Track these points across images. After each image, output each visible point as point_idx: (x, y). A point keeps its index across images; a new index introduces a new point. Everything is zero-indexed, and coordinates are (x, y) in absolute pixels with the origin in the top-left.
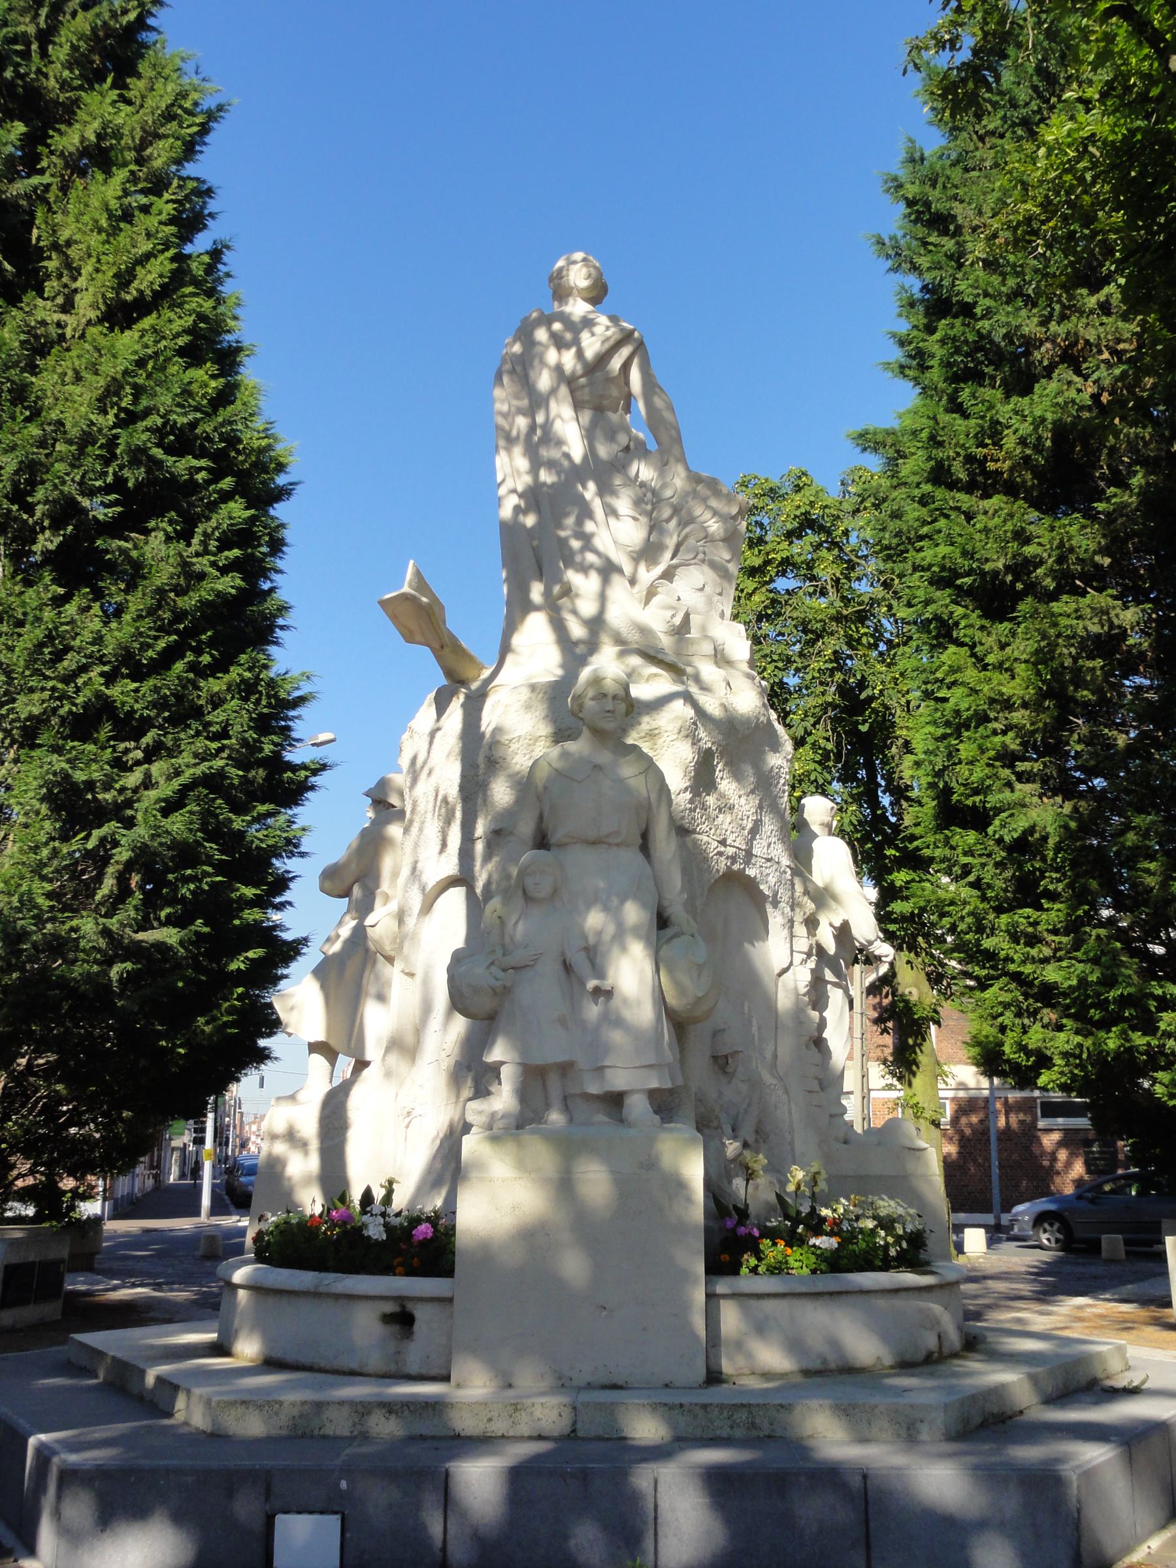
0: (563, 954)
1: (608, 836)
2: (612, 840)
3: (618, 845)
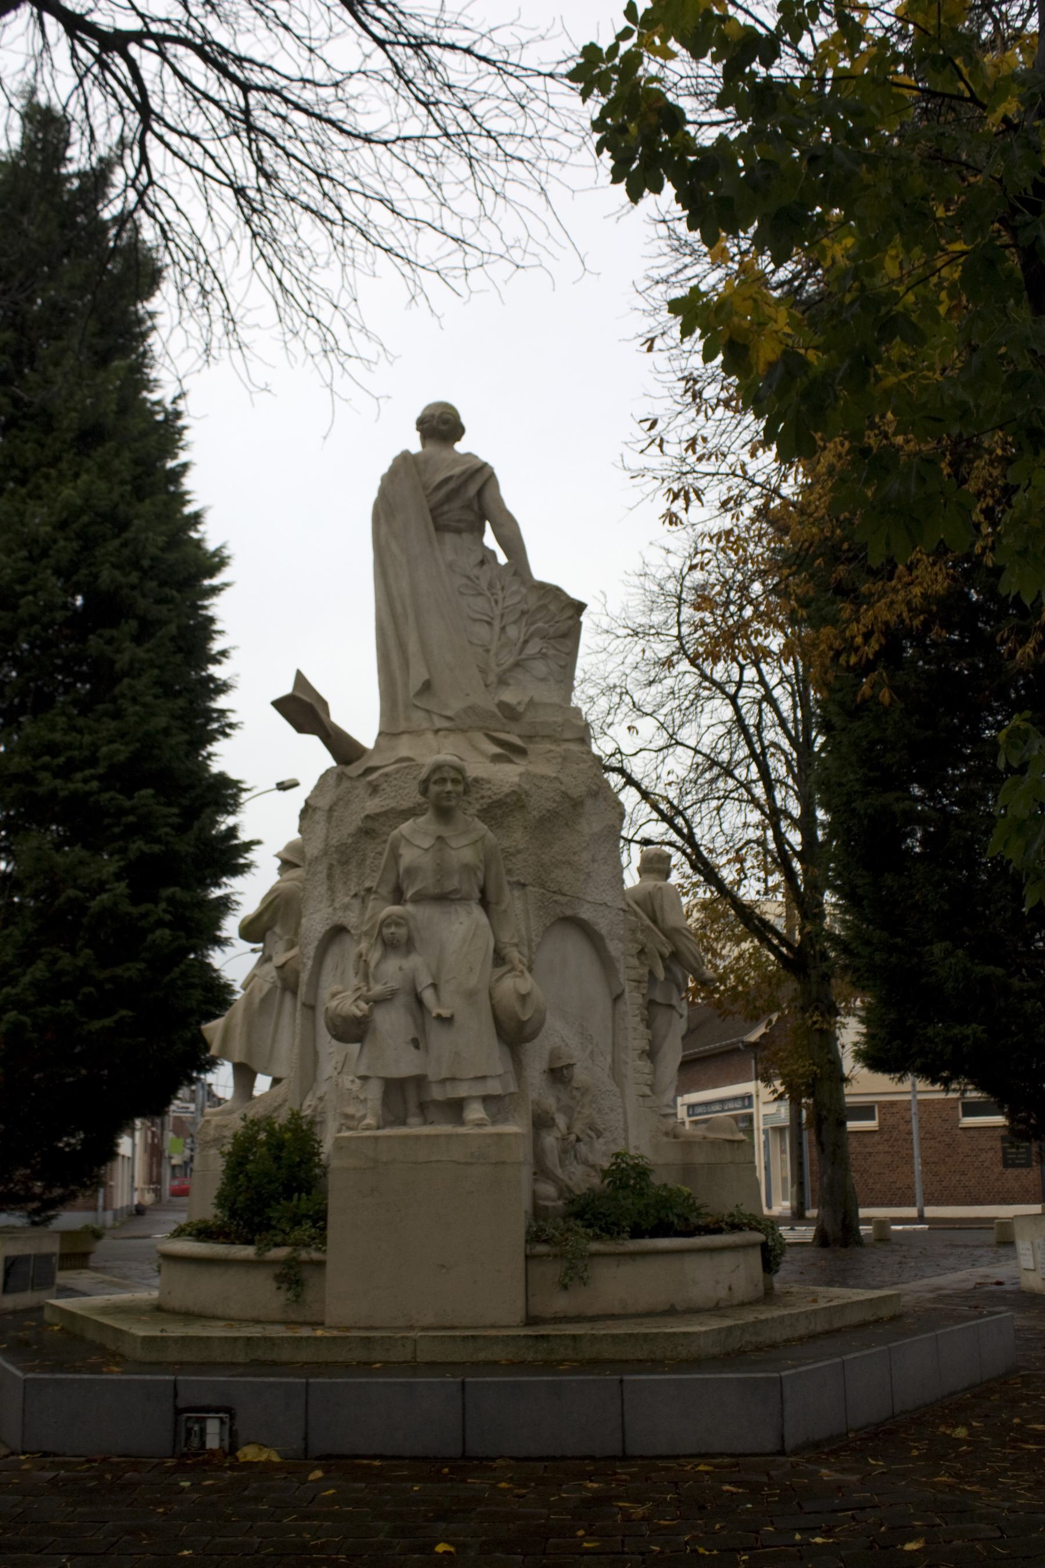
0: (415, 989)
1: (450, 893)
2: (453, 897)
3: (460, 899)
